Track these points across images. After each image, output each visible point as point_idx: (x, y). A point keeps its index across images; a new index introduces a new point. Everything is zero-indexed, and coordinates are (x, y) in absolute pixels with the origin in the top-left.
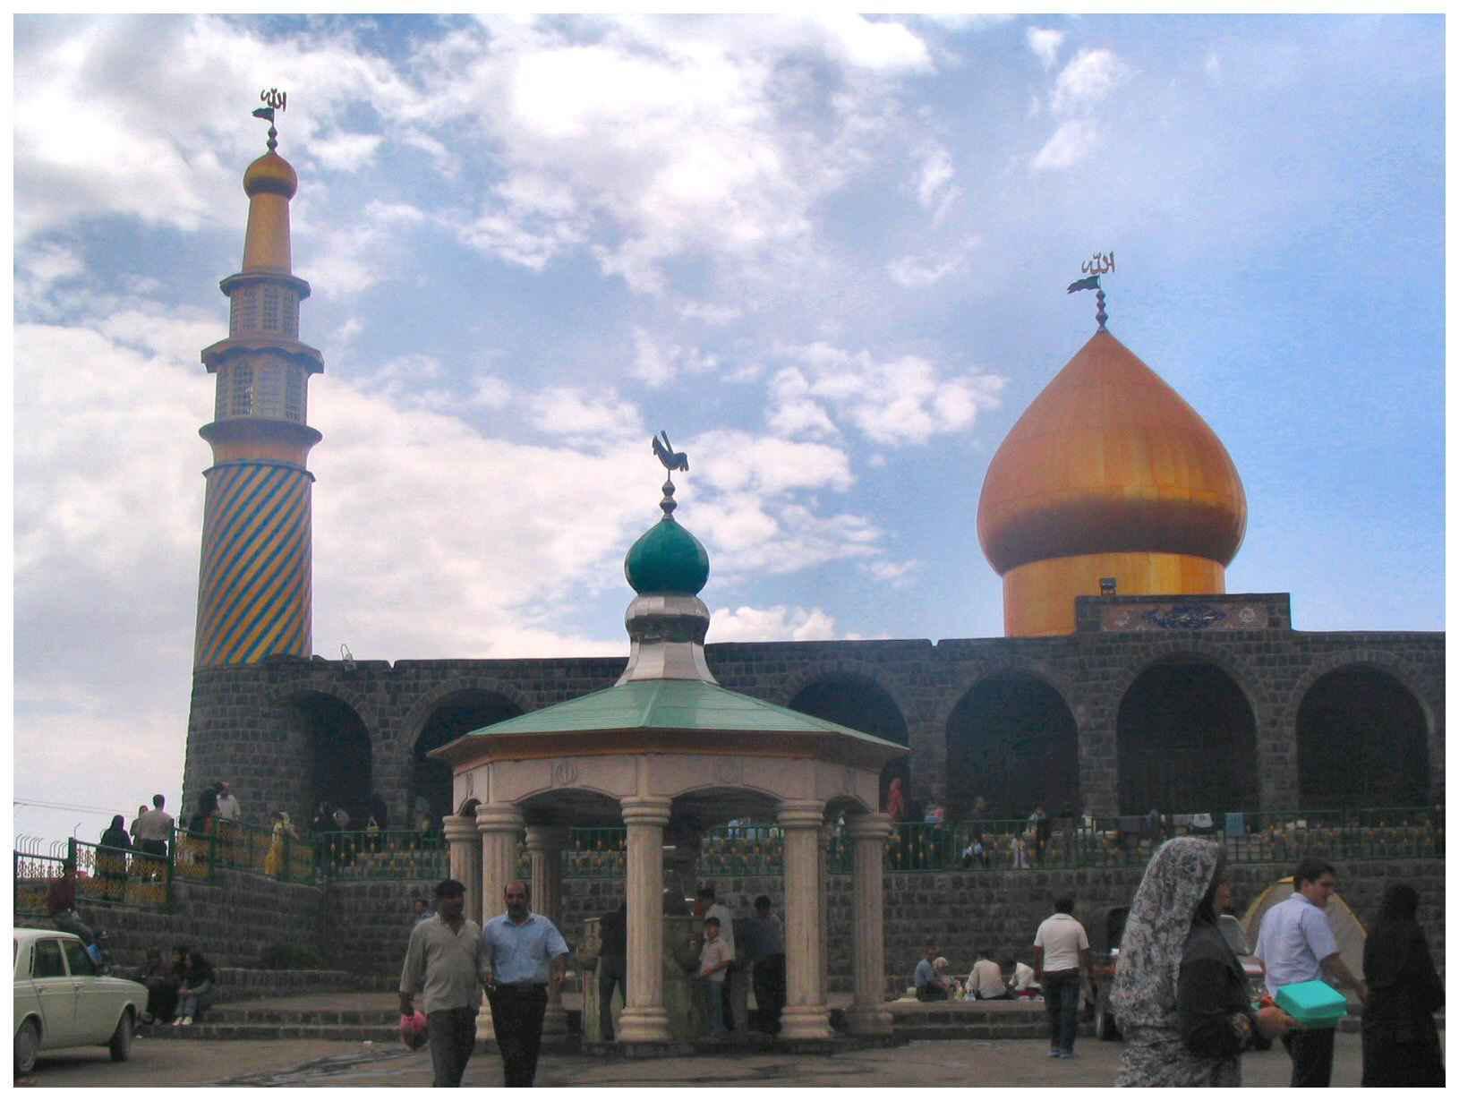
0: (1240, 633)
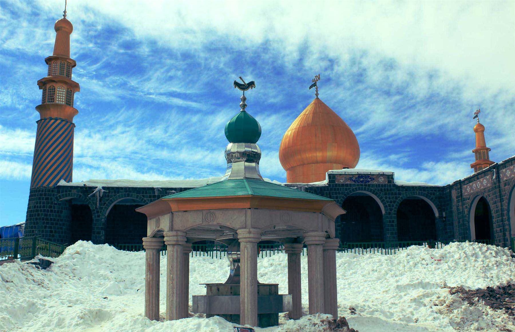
0: (379, 185)
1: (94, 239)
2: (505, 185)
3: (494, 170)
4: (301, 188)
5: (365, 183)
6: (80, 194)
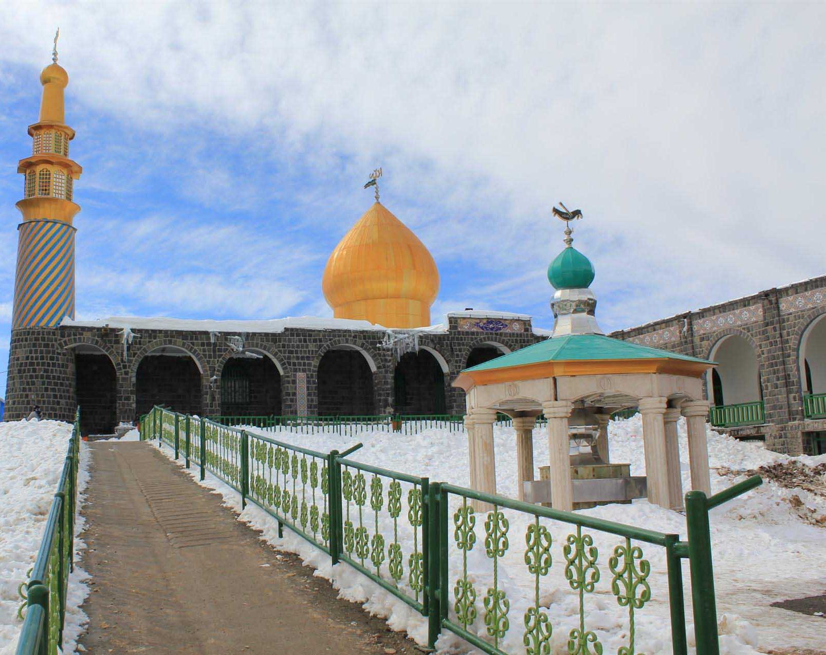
0: (513, 334)
1: (121, 407)
2: (702, 339)
3: (685, 320)
4: (413, 335)
5: (496, 331)
6: (96, 338)
